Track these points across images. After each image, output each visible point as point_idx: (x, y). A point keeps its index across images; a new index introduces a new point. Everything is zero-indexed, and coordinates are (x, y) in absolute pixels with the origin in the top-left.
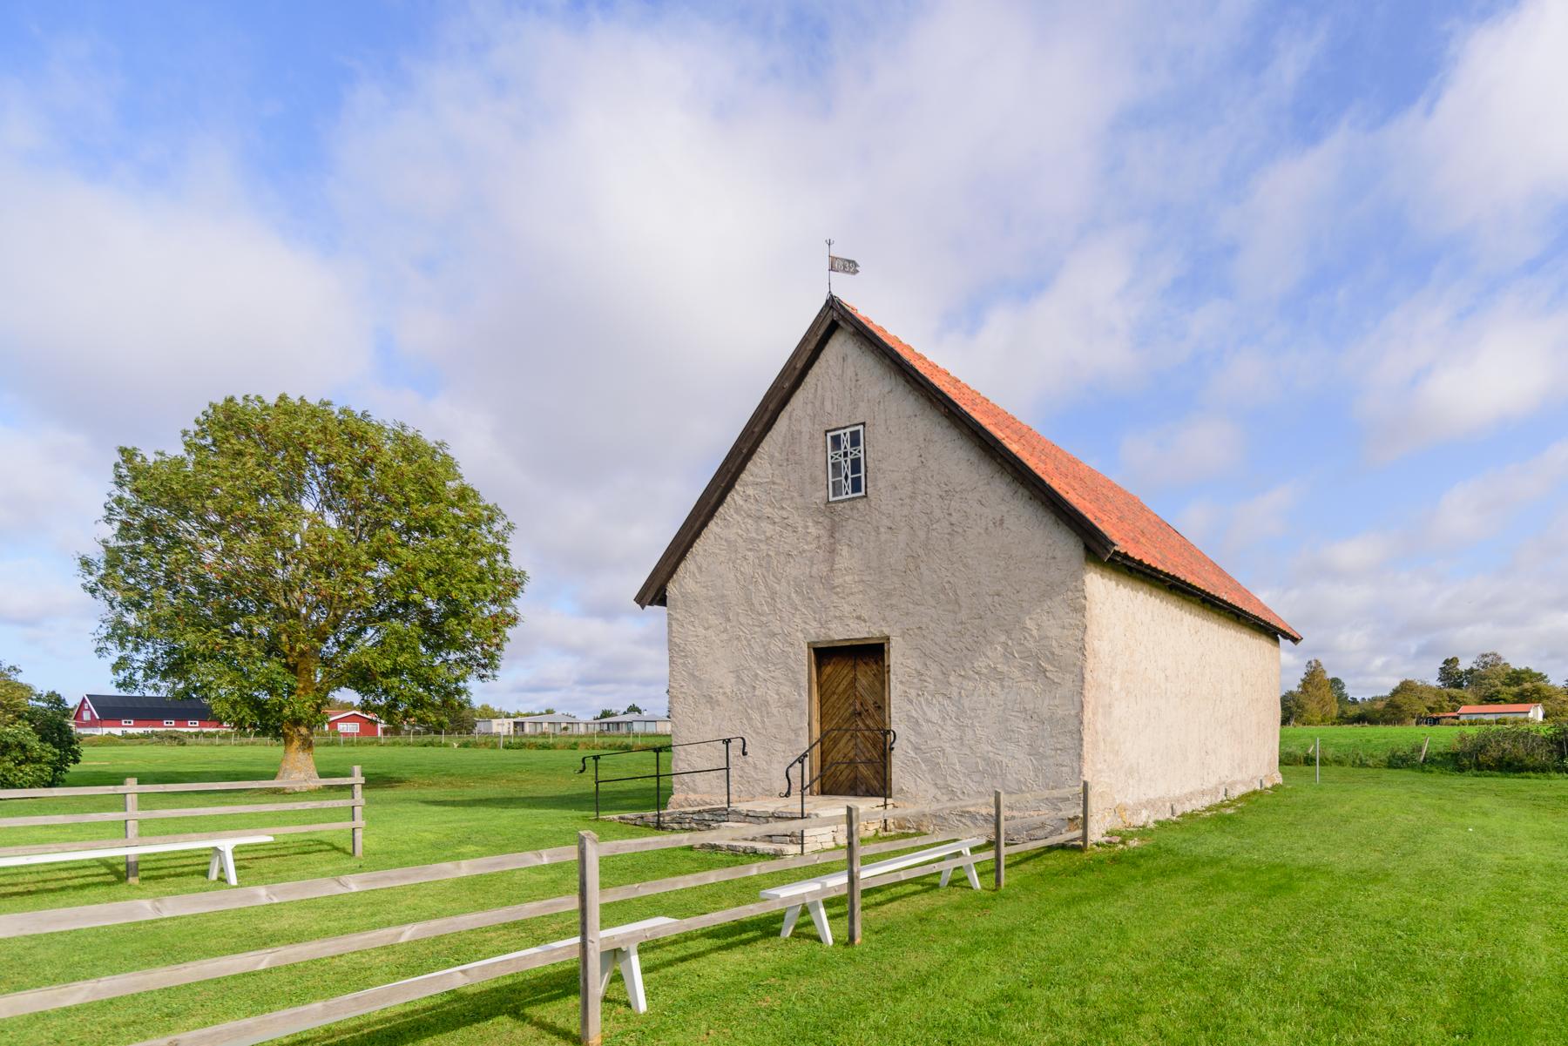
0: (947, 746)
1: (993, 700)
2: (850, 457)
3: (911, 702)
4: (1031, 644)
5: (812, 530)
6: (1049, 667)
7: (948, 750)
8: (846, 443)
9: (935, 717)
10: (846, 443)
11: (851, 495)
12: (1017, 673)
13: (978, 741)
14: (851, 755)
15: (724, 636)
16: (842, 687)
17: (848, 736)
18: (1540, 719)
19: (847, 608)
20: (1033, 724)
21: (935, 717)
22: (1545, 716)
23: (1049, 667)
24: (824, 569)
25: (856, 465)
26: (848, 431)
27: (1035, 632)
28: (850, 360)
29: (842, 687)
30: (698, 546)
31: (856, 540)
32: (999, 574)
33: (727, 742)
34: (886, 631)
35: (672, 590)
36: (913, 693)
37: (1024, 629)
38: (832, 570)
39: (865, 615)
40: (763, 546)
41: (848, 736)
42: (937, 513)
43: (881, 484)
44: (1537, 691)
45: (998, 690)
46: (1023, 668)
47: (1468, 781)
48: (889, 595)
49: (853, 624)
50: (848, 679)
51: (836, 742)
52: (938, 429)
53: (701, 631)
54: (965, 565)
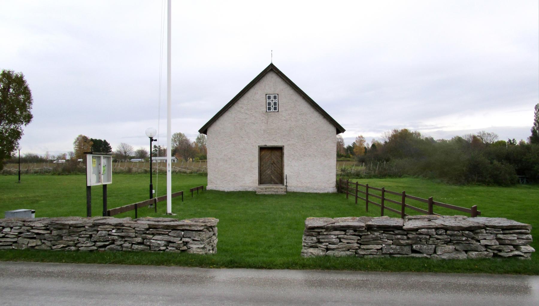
8: (272, 98)
10: (272, 98)
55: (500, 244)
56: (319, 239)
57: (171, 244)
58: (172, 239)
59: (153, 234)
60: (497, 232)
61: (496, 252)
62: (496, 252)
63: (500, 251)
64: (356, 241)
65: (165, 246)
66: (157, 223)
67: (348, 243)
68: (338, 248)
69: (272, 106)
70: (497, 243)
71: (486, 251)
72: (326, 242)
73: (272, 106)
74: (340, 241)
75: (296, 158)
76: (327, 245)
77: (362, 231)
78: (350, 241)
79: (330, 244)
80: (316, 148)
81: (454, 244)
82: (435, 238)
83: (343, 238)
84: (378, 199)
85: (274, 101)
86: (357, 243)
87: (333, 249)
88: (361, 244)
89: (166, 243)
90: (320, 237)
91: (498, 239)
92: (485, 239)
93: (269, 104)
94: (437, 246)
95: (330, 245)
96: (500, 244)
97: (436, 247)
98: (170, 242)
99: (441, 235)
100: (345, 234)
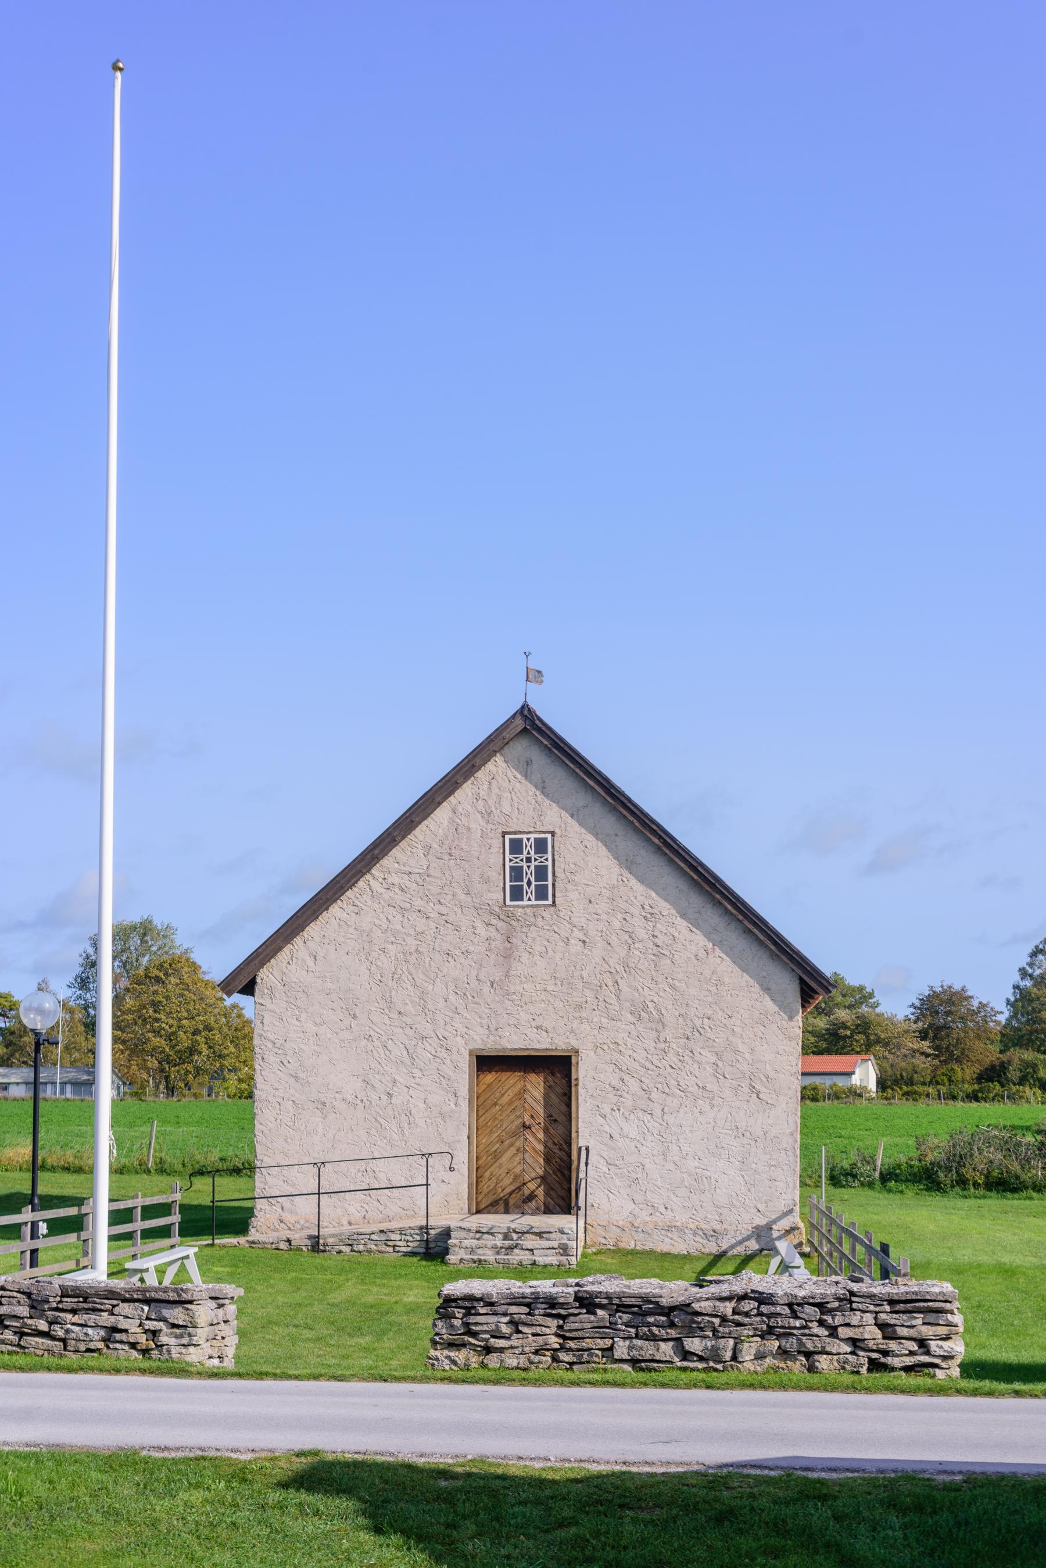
0: (647, 1162)
1: (701, 1118)
2: (524, 856)
3: (604, 1117)
4: (745, 1067)
5: (481, 929)
6: (763, 1090)
7: (648, 1166)
8: (528, 849)
9: (633, 1133)
10: (528, 849)
11: (534, 902)
12: (728, 1093)
13: (684, 1158)
14: (518, 1170)
15: (346, 1035)
16: (505, 1099)
17: (513, 1150)
18: (872, 1085)
19: (524, 1017)
20: (745, 1141)
21: (633, 1133)
22: (882, 1084)
23: (763, 1090)
24: (497, 975)
25: (541, 873)
26: (532, 836)
27: (747, 1056)
28: (535, 766)
29: (505, 1099)
30: (313, 930)
31: (538, 948)
32: (710, 999)
33: (427, 1156)
34: (575, 1043)
35: (266, 976)
36: (606, 1109)
37: (736, 1051)
38: (507, 976)
39: (547, 1024)
40: (411, 941)
41: (513, 1150)
42: (641, 933)
43: (573, 896)
44: (864, 1026)
45: (707, 1108)
46: (736, 1090)
47: (972, 1202)
48: (579, 1007)
49: (532, 1033)
50: (516, 1090)
51: (496, 1156)
52: (643, 852)
53: (310, 1027)
54: (672, 987)
55: (884, 1338)
56: (469, 1324)
57: (118, 1336)
58: (123, 1324)
59: (74, 1312)
60: (877, 1309)
61: (874, 1355)
62: (874, 1355)
63: (885, 1353)
64: (554, 1330)
65: (104, 1340)
66: (624, 1468)
67: (534, 1335)
68: (512, 1347)
69: (530, 875)
70: (879, 1334)
71: (853, 1353)
72: (486, 1332)
73: (530, 875)
74: (519, 1332)
75: (629, 1103)
76: (487, 1340)
77: (562, 1305)
78: (538, 1330)
79: (493, 1337)
80: (713, 1058)
81: (779, 1337)
82: (733, 1321)
83: (525, 1324)
84: (17, 1175)
85: (520, 860)
86: (557, 1335)
87: (501, 1350)
88: (565, 1338)
89: (102, 1333)
90: (472, 1319)
91: (882, 1326)
92: (848, 1325)
93: (517, 873)
94: (738, 1341)
95: (492, 1340)
96: (884, 1338)
97: (736, 1344)
98: (115, 1330)
99: (747, 1314)
100: (529, 1314)
